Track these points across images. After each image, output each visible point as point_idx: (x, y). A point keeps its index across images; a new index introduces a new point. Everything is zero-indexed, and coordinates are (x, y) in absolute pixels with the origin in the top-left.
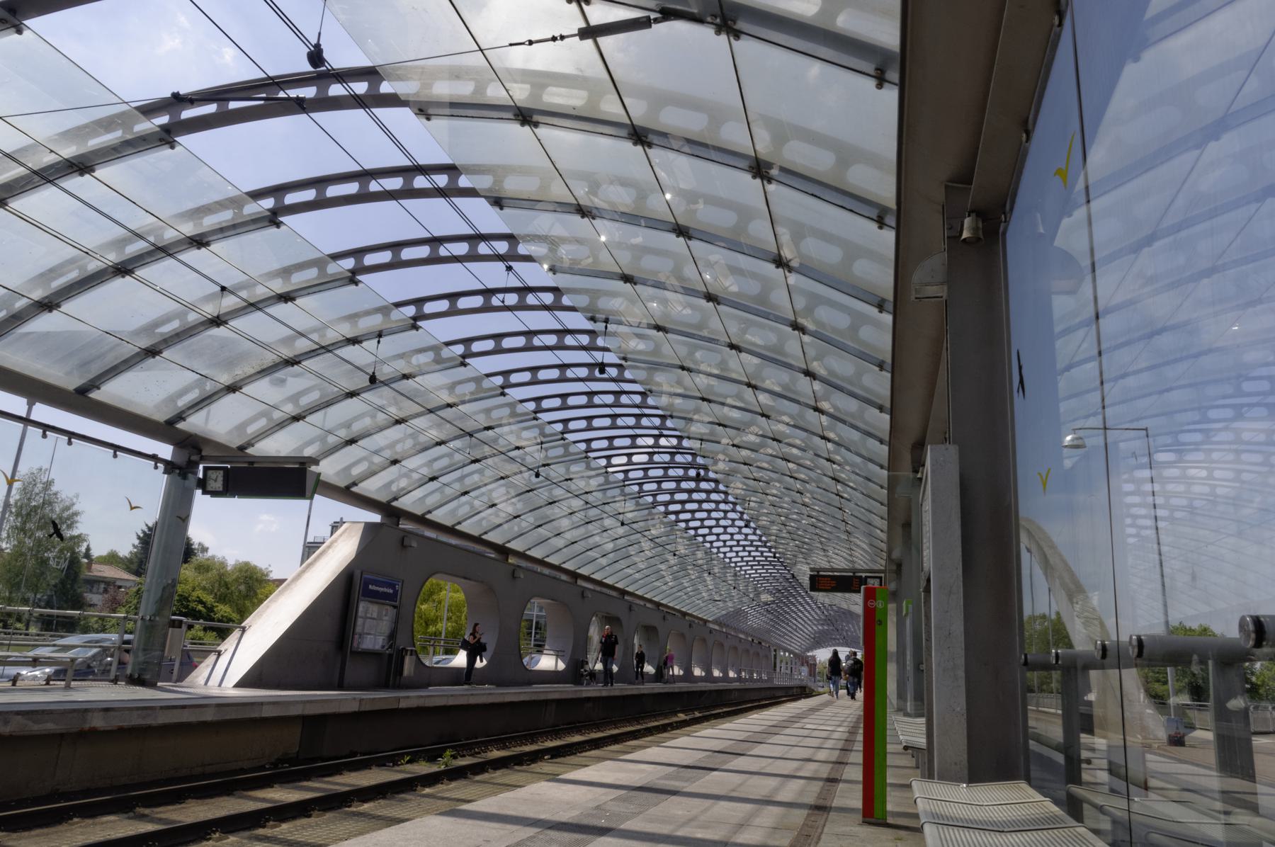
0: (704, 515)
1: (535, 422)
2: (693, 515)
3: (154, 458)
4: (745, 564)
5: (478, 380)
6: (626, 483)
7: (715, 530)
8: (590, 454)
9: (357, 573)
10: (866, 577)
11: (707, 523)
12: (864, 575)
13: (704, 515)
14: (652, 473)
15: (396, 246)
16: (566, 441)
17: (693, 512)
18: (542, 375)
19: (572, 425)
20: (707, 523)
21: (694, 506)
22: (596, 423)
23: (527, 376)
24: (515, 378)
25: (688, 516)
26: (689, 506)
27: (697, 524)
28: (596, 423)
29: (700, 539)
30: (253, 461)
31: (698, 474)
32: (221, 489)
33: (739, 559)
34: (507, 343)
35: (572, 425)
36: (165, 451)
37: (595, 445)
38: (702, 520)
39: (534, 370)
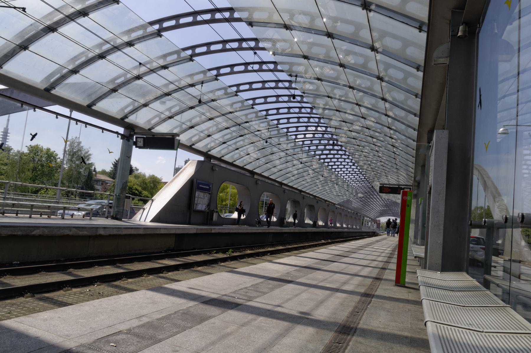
0: (336, 160)
1: (266, 120)
2: (331, 160)
3: (117, 133)
4: (352, 181)
5: (242, 102)
6: (303, 146)
7: (340, 167)
8: (288, 134)
9: (195, 180)
11: (337, 163)
13: (336, 160)
14: (314, 142)
15: (208, 44)
16: (279, 128)
17: (331, 159)
18: (269, 100)
19: (281, 121)
20: (337, 163)
21: (332, 156)
22: (291, 120)
23: (262, 100)
24: (257, 101)
25: (329, 160)
26: (329, 156)
27: (333, 164)
28: (291, 120)
29: (334, 170)
30: (154, 134)
31: (334, 143)
32: (142, 146)
33: (350, 179)
34: (254, 86)
35: (281, 121)
36: (121, 130)
37: (290, 130)
38: (335, 162)
39: (266, 97)
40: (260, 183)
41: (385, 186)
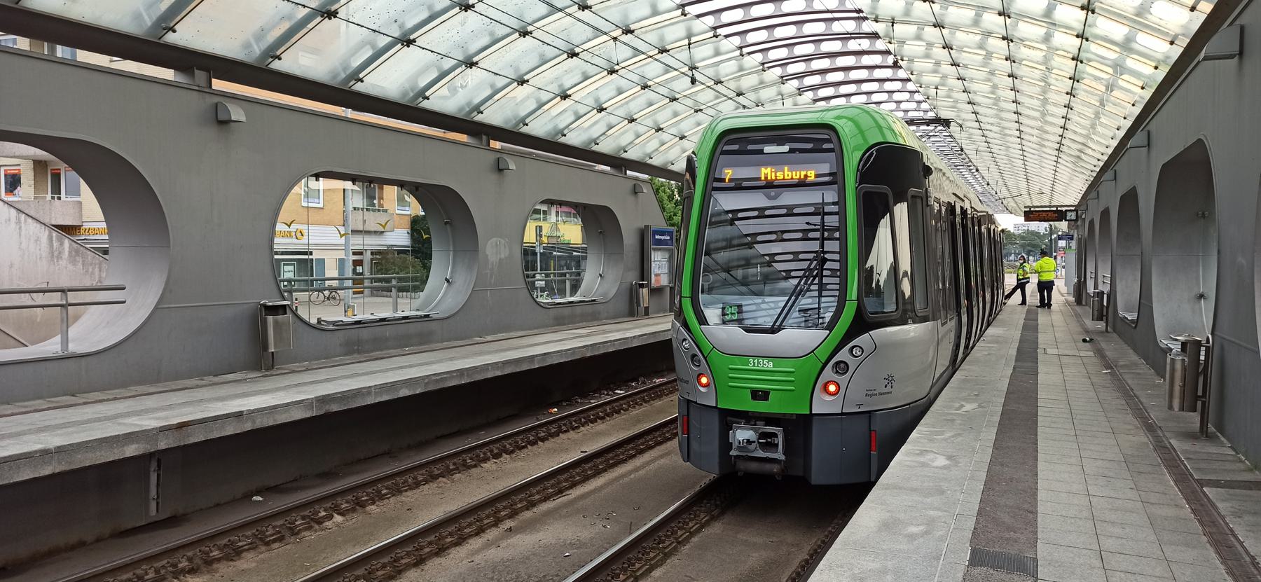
10: (1066, 211)
12: (1064, 209)
16: (688, 16)
23: (738, 15)
24: (726, 17)
40: (512, 166)
41: (1059, 209)
